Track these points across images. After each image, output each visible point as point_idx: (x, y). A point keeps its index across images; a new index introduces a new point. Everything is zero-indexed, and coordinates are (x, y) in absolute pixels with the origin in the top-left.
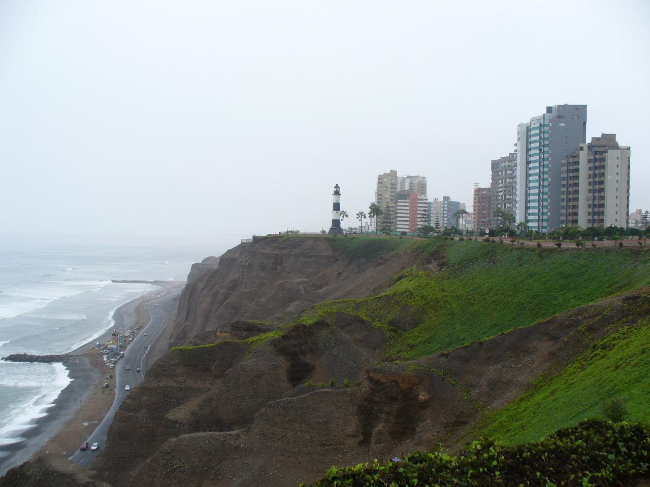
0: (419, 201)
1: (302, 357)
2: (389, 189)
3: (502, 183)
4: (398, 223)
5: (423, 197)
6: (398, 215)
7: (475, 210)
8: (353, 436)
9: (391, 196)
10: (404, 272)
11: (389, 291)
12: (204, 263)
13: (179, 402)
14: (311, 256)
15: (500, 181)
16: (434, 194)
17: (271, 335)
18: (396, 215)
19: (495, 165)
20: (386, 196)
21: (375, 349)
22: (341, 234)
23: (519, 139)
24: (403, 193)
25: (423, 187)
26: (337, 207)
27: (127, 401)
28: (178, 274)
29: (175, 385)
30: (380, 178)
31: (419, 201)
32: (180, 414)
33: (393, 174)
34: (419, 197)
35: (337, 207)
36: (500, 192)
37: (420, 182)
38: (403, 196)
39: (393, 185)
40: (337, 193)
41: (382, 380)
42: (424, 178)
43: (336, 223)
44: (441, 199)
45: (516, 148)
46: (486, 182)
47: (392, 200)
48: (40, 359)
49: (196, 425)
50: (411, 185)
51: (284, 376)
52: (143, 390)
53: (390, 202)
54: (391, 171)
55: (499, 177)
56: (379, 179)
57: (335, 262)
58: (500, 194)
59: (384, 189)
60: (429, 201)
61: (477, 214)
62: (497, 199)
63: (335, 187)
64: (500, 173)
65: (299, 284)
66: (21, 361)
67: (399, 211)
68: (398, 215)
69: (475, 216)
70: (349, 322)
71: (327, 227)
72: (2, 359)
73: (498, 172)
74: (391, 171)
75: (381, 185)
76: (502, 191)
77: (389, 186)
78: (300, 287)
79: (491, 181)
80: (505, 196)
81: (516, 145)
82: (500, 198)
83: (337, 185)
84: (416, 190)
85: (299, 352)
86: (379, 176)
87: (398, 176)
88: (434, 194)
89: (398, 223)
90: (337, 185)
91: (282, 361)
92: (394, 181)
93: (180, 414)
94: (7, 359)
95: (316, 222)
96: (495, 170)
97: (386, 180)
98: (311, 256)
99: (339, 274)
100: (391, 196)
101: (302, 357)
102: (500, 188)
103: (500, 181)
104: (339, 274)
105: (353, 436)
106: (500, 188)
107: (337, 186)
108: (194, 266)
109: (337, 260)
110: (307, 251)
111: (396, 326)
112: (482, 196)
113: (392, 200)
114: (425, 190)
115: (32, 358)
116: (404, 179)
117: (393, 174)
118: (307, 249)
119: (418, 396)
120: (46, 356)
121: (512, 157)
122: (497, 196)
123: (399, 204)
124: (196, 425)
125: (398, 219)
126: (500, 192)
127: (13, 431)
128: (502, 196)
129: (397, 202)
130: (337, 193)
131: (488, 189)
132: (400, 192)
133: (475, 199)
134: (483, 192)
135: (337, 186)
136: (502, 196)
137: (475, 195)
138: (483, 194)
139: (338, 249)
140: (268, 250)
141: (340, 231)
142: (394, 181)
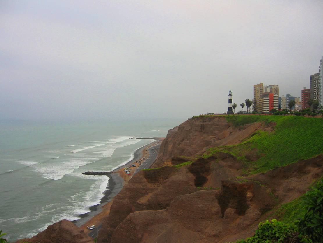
0: (274, 97)
1: (202, 174)
2: (259, 92)
3: (316, 86)
4: (264, 108)
5: (276, 95)
6: (264, 104)
7: (302, 100)
8: (216, 214)
9: (260, 95)
10: (256, 132)
11: (250, 140)
12: (174, 129)
13: (144, 194)
14: (218, 125)
15: (314, 86)
16: (282, 93)
17: (186, 163)
18: (263, 104)
19: (312, 78)
20: (258, 95)
21: (238, 170)
22: (232, 114)
23: (321, 64)
24: (266, 93)
25: (277, 91)
26: (230, 101)
27: (119, 194)
28: (163, 133)
29: (141, 187)
30: (255, 87)
31: (274, 97)
32: (143, 200)
33: (261, 85)
34: (274, 95)
35: (230, 101)
36: (315, 91)
37: (275, 88)
38: (266, 95)
39: (261, 90)
40: (230, 95)
41: (229, 186)
42: (277, 86)
43: (230, 109)
44: (285, 96)
45: (320, 68)
46: (308, 87)
47: (261, 97)
48: (98, 174)
49: (149, 206)
50: (271, 89)
51: (192, 183)
52: (127, 189)
53: (260, 98)
54: (260, 83)
55: (314, 84)
56: (254, 87)
57: (229, 128)
58: (315, 92)
59: (257, 92)
60: (279, 97)
61: (303, 102)
62: (313, 95)
63: (229, 92)
64: (314, 82)
65: (211, 138)
66: (90, 175)
67: (264, 102)
68: (264, 104)
69: (303, 103)
70: (225, 157)
71: (226, 111)
72: (82, 174)
73: (313, 81)
74: (260, 83)
75: (255, 90)
76: (316, 91)
77: (259, 90)
78: (212, 139)
79: (310, 86)
80: (317, 93)
81: (320, 67)
82: (314, 94)
83: (230, 91)
84: (273, 92)
85: (200, 171)
86: (254, 86)
87: (263, 85)
88: (282, 93)
89: (264, 108)
90: (230, 91)
91: (191, 175)
92: (261, 88)
93: (143, 200)
94: (84, 174)
95: (221, 109)
96: (312, 80)
97: (257, 88)
98: (218, 125)
99: (230, 133)
100: (260, 95)
101: (202, 174)
102: (315, 89)
103: (314, 86)
104: (230, 133)
105: (216, 214)
106: (315, 89)
107: (230, 92)
108: (170, 131)
109: (230, 127)
110: (215, 123)
111: (249, 159)
112: (305, 93)
113: (261, 97)
114: (278, 92)
115: (95, 173)
116: (267, 87)
117: (261, 85)
118: (215, 122)
119: (247, 195)
120: (101, 172)
121: (317, 75)
122: (313, 93)
123: (264, 99)
124: (149, 206)
125: (264, 106)
126: (315, 91)
127: (90, 207)
128: (316, 93)
129: (263, 98)
130: (230, 95)
131: (309, 90)
132: (265, 93)
133: (302, 95)
134: (306, 92)
135: (230, 92)
136: (316, 93)
137: (302, 93)
138: (306, 92)
139: (232, 121)
140: (198, 123)
141: (232, 113)
142: (261, 88)
